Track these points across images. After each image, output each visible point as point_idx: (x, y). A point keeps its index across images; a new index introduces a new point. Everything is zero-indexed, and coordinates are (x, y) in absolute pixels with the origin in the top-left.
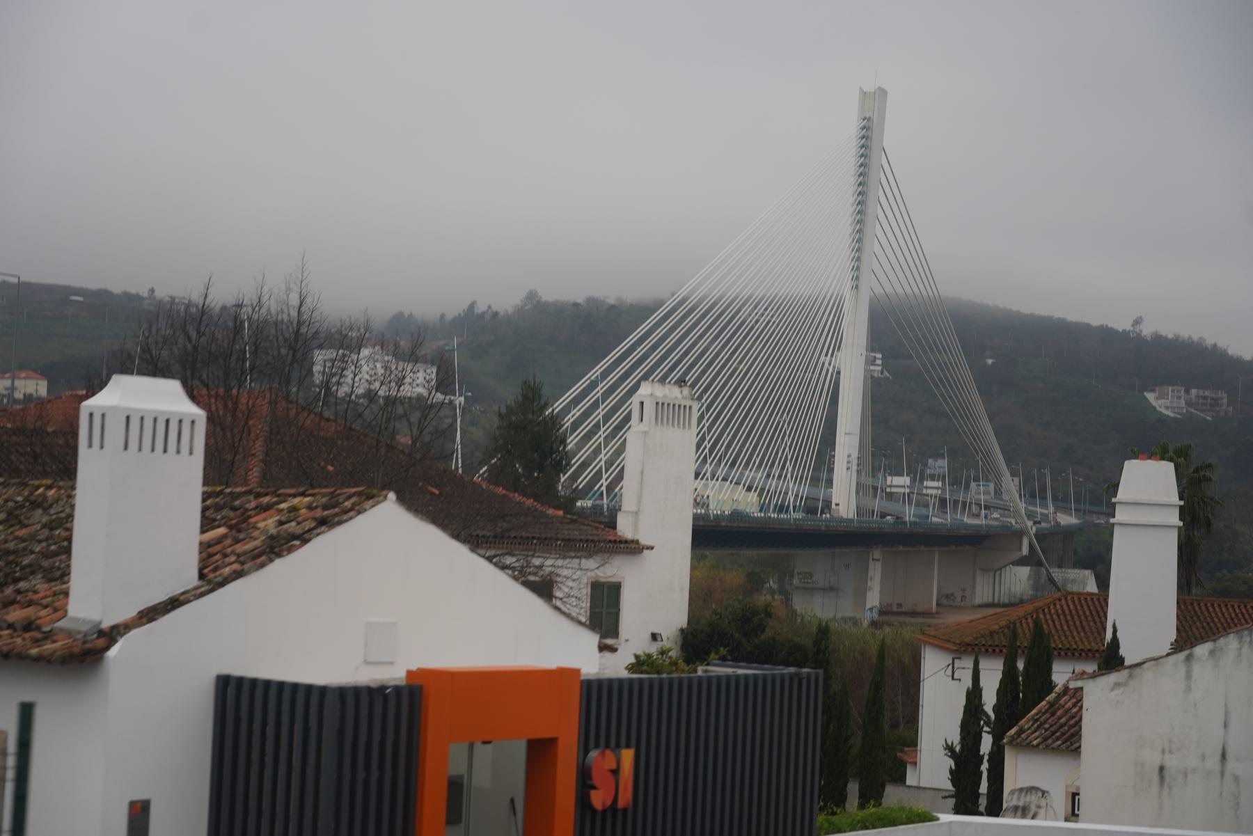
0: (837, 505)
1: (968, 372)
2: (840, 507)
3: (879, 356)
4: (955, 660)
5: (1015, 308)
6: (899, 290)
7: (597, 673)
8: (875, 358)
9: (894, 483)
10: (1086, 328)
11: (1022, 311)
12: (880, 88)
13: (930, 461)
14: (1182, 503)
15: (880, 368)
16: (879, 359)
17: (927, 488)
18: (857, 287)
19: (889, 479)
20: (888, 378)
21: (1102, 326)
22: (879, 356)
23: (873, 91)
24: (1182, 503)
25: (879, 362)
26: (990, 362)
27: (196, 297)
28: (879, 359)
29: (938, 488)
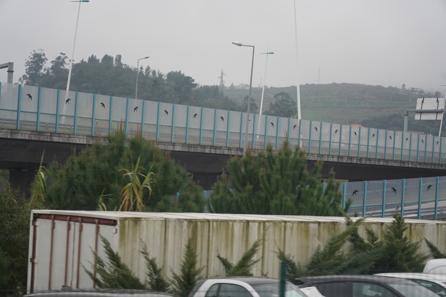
4: (253, 47)
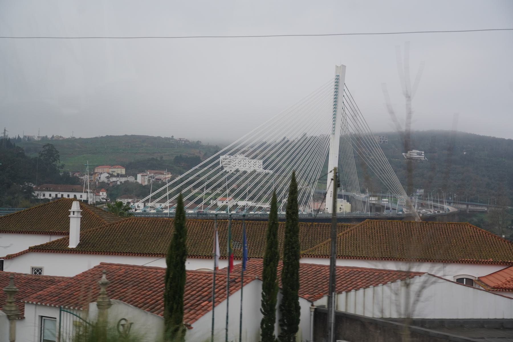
0: (327, 209)
1: (196, 170)
2: (328, 209)
3: (423, 152)
5: (472, 133)
6: (364, 132)
7: (434, 267)
8: (422, 153)
9: (372, 200)
10: (503, 140)
11: (480, 135)
12: (342, 65)
13: (418, 190)
14: (81, 216)
15: (423, 157)
16: (423, 153)
17: (383, 201)
18: (334, 134)
19: (370, 198)
20: (426, 160)
21: (509, 139)
22: (423, 152)
23: (340, 66)
24: (81, 216)
25: (423, 154)
26: (465, 153)
27: (403, 129)
28: (423, 153)
29: (387, 201)
